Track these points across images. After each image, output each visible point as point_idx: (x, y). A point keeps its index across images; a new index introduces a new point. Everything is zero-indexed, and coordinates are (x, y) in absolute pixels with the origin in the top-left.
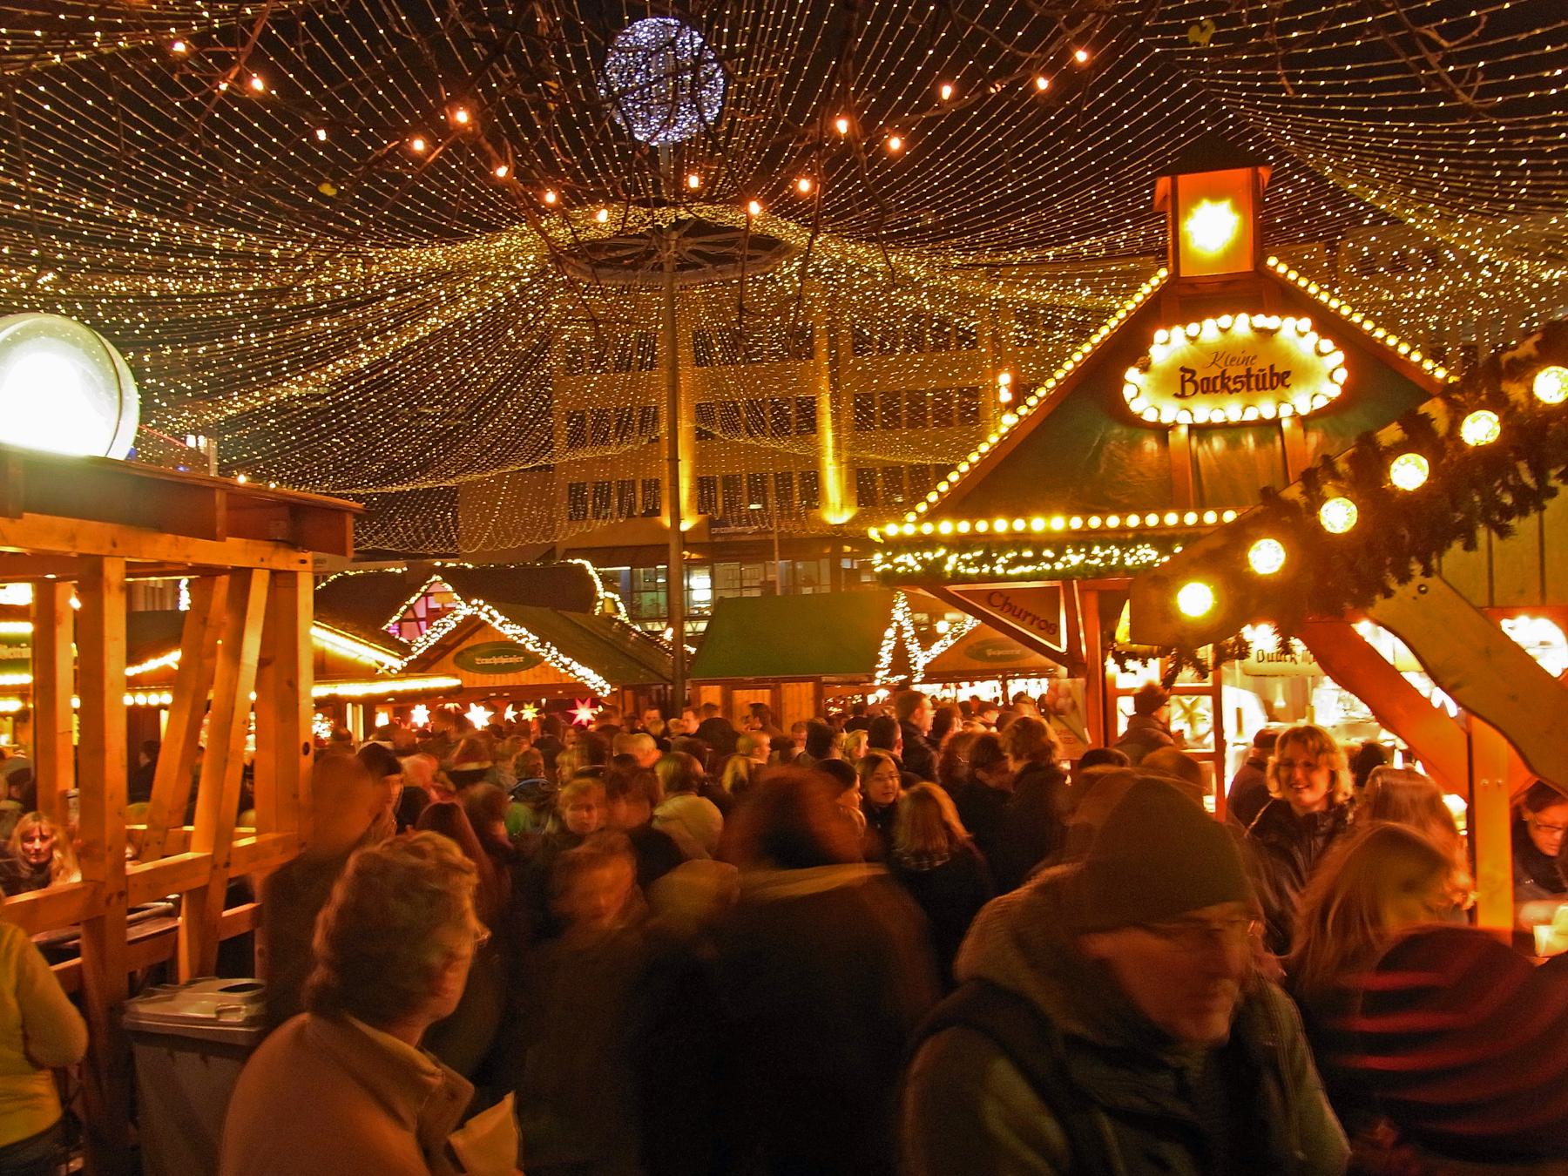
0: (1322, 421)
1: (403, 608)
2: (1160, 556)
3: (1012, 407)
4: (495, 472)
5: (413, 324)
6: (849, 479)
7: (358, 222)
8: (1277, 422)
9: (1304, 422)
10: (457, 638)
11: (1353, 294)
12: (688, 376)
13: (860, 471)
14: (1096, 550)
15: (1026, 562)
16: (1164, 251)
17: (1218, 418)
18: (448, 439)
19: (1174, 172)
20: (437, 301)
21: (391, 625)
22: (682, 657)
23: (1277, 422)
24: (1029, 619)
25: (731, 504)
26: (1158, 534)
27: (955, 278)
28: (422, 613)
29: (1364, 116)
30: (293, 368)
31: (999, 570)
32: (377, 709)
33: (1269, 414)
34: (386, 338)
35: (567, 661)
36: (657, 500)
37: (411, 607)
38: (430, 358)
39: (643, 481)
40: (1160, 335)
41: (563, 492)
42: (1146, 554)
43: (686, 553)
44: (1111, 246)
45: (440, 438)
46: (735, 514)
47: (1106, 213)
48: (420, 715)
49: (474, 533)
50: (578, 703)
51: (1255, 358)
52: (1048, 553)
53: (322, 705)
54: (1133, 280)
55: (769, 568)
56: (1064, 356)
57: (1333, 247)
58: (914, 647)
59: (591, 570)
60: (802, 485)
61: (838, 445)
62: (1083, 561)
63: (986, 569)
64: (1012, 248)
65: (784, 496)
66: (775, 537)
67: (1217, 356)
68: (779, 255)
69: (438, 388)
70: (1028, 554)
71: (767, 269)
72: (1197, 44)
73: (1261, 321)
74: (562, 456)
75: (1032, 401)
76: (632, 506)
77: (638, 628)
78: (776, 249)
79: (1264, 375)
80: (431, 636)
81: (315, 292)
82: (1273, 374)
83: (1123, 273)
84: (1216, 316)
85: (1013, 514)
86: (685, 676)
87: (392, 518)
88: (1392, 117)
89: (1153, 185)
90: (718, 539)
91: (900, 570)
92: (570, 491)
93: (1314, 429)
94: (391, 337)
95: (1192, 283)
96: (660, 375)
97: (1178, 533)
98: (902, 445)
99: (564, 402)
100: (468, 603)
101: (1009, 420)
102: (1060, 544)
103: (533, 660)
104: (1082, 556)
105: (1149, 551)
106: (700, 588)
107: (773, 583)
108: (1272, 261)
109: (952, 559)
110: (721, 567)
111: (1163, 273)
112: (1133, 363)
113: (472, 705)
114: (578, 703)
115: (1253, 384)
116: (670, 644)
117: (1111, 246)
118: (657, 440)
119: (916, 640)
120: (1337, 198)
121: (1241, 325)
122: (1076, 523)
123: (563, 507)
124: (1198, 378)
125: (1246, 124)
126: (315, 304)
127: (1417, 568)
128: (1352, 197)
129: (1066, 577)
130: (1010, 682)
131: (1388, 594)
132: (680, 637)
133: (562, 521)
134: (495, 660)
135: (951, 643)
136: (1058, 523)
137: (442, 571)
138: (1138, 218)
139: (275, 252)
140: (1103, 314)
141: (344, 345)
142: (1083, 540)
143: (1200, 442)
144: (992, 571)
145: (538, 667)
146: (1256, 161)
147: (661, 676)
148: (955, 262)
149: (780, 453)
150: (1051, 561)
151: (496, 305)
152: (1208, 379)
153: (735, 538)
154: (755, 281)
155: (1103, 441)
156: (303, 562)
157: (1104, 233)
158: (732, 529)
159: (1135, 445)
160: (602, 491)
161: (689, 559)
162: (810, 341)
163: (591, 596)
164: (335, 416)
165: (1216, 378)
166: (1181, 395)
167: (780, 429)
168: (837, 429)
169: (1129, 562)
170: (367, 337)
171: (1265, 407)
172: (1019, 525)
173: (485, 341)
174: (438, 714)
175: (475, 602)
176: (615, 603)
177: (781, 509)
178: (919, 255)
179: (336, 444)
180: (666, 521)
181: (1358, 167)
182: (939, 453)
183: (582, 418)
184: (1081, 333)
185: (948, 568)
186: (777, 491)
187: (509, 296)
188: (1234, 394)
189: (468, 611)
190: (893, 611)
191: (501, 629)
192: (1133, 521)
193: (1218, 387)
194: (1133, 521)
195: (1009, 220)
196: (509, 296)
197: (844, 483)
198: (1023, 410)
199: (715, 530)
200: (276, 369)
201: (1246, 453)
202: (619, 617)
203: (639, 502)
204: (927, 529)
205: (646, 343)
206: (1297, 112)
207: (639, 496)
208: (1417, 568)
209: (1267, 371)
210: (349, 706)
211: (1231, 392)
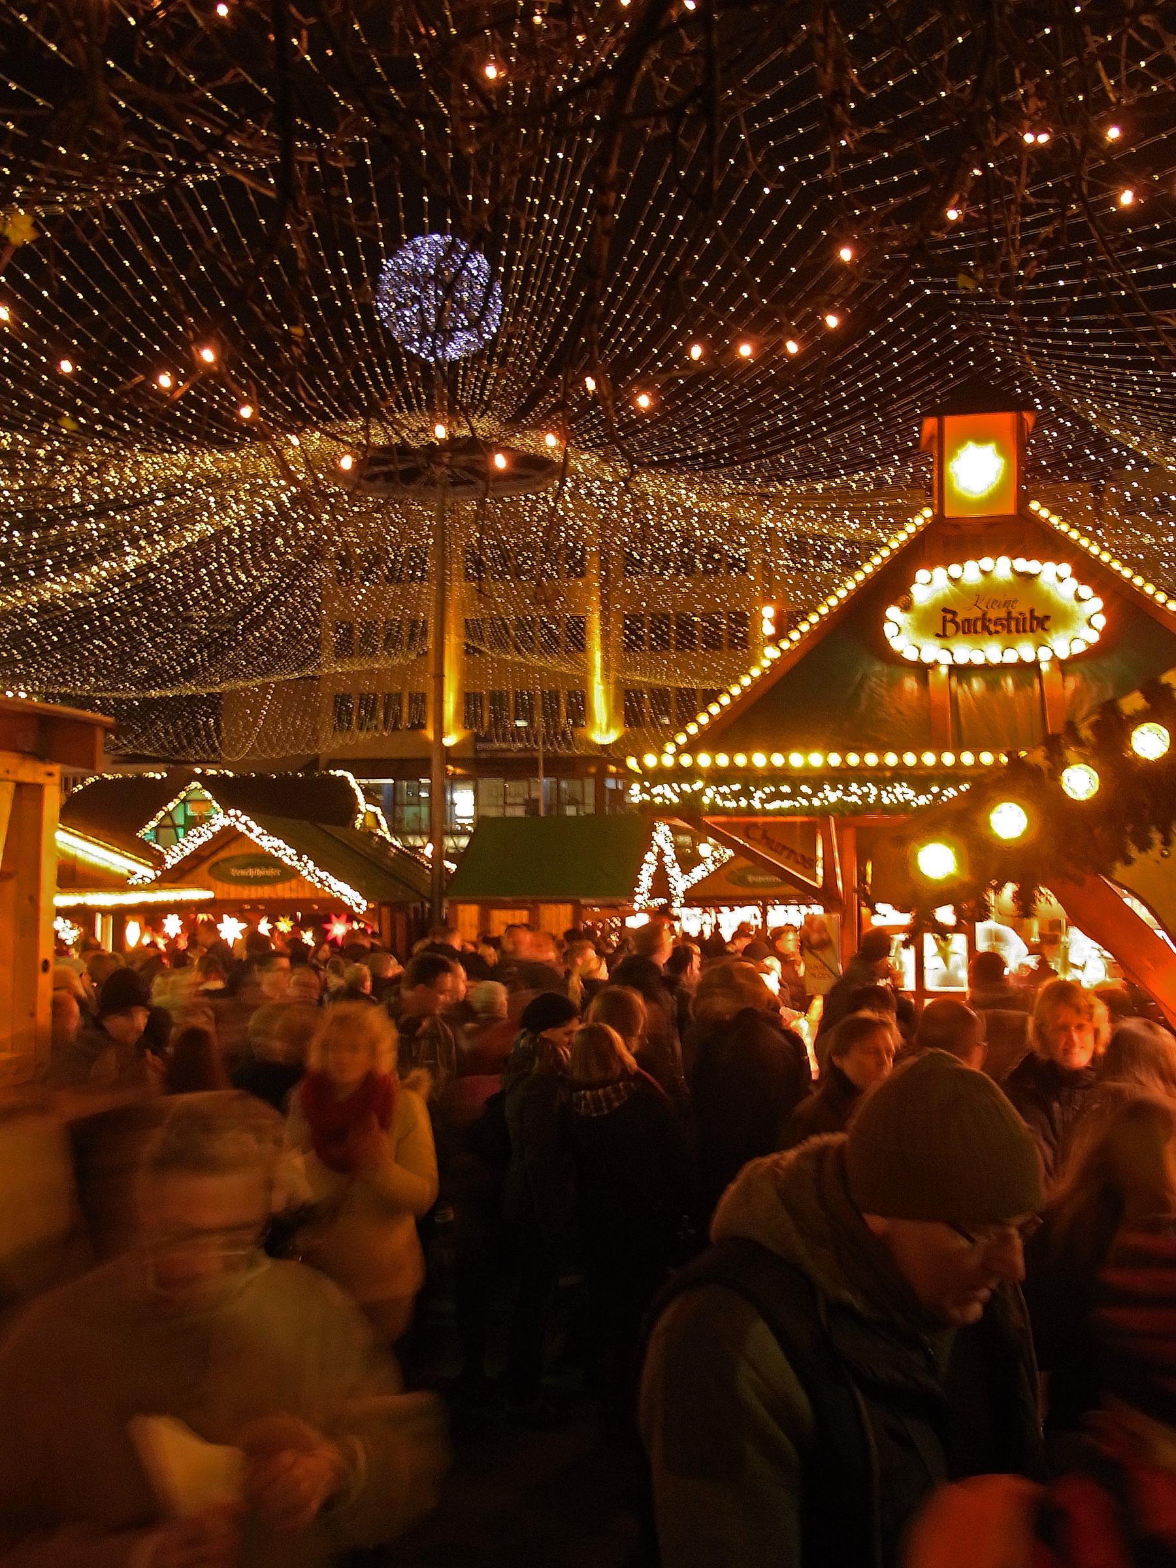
0: (1080, 666)
1: (161, 814)
3: (774, 640)
4: (259, 681)
5: (183, 528)
6: (616, 700)
7: (126, 426)
8: (1036, 664)
9: (1063, 666)
10: (214, 848)
11: (1117, 536)
12: (458, 590)
13: (627, 692)
14: (854, 787)
16: (930, 488)
17: (978, 659)
18: (214, 647)
19: (939, 412)
20: (206, 506)
21: (146, 832)
22: (441, 877)
23: (1036, 664)
25: (497, 721)
26: (915, 773)
27: (725, 505)
28: (180, 820)
29: (1125, 365)
30: (57, 569)
31: (757, 804)
32: (128, 918)
33: (1029, 657)
34: (153, 543)
35: (323, 875)
36: (422, 714)
37: (169, 814)
38: (198, 564)
39: (410, 695)
40: (922, 575)
41: (328, 703)
42: (903, 792)
43: (450, 768)
45: (204, 644)
46: (500, 732)
47: (875, 449)
48: (173, 925)
49: (238, 740)
50: (334, 918)
51: (1016, 601)
52: (805, 789)
53: (65, 913)
54: (901, 515)
55: (533, 786)
56: (829, 588)
57: (1096, 490)
58: (675, 872)
59: (353, 782)
60: (570, 703)
61: (606, 666)
62: (840, 799)
63: (743, 803)
64: (782, 479)
65: (552, 715)
66: (540, 756)
67: (978, 596)
69: (204, 594)
70: (786, 789)
71: (538, 488)
72: (965, 289)
73: (1021, 565)
74: (332, 667)
75: (795, 635)
76: (398, 719)
77: (398, 844)
78: (549, 470)
79: (1024, 619)
80: (190, 844)
81: (81, 493)
82: (1033, 617)
83: (891, 508)
84: (978, 558)
85: (770, 750)
86: (443, 894)
87: (153, 723)
88: (1154, 366)
89: (919, 425)
90: (483, 755)
91: (658, 800)
92: (336, 701)
93: (1073, 674)
94: (158, 542)
95: (956, 523)
96: (428, 589)
97: (935, 772)
98: (669, 669)
99: (331, 611)
100: (226, 813)
101: (772, 653)
102: (817, 780)
103: (290, 874)
104: (839, 793)
105: (906, 790)
106: (464, 803)
107: (537, 801)
109: (710, 792)
110: (484, 783)
111: (928, 513)
112: (894, 602)
113: (225, 917)
114: (334, 918)
115: (1013, 627)
116: (429, 861)
117: (879, 482)
118: (425, 653)
119: (676, 865)
120: (1100, 444)
121: (1002, 568)
122: (835, 759)
123: (328, 719)
125: (1014, 367)
126: (81, 506)
127: (1156, 837)
128: (1115, 442)
129: (825, 812)
130: (769, 908)
131: (1128, 861)
132: (440, 854)
133: (326, 733)
134: (251, 872)
135: (712, 868)
136: (816, 759)
137: (202, 778)
138: (906, 454)
139: (41, 452)
140: (876, 545)
141: (111, 547)
142: (841, 777)
143: (960, 682)
144: (749, 804)
145: (294, 882)
146: (1021, 405)
147: (418, 892)
148: (726, 491)
149: (547, 671)
150: (807, 797)
151: (266, 513)
152: (968, 620)
153: (500, 755)
154: (527, 499)
155: (865, 677)
156: (50, 774)
157: (873, 468)
158: (497, 745)
159: (896, 683)
160: (370, 703)
161: (454, 774)
162: (580, 563)
163: (353, 810)
164: (100, 618)
166: (942, 635)
167: (551, 645)
168: (605, 649)
169: (886, 801)
170: (134, 542)
171: (1025, 651)
172: (778, 760)
173: (252, 550)
174: (189, 926)
175: (232, 812)
176: (375, 815)
177: (547, 727)
178: (690, 482)
179: (98, 647)
180: (430, 734)
181: (1121, 415)
182: (707, 677)
183: (350, 630)
184: (850, 565)
185: (706, 800)
186: (544, 708)
187: (279, 505)
189: (226, 822)
190: (654, 834)
191: (257, 841)
192: (891, 759)
193: (979, 628)
194: (891, 759)
195: (779, 451)
196: (279, 505)
197: (612, 704)
198: (785, 645)
199: (480, 746)
200: (40, 569)
201: (1006, 696)
202: (380, 833)
203: (405, 715)
204: (686, 760)
205: (416, 558)
206: (1062, 357)
207: (405, 709)
208: (1156, 837)
209: (1028, 615)
210: (99, 917)
211: (990, 633)
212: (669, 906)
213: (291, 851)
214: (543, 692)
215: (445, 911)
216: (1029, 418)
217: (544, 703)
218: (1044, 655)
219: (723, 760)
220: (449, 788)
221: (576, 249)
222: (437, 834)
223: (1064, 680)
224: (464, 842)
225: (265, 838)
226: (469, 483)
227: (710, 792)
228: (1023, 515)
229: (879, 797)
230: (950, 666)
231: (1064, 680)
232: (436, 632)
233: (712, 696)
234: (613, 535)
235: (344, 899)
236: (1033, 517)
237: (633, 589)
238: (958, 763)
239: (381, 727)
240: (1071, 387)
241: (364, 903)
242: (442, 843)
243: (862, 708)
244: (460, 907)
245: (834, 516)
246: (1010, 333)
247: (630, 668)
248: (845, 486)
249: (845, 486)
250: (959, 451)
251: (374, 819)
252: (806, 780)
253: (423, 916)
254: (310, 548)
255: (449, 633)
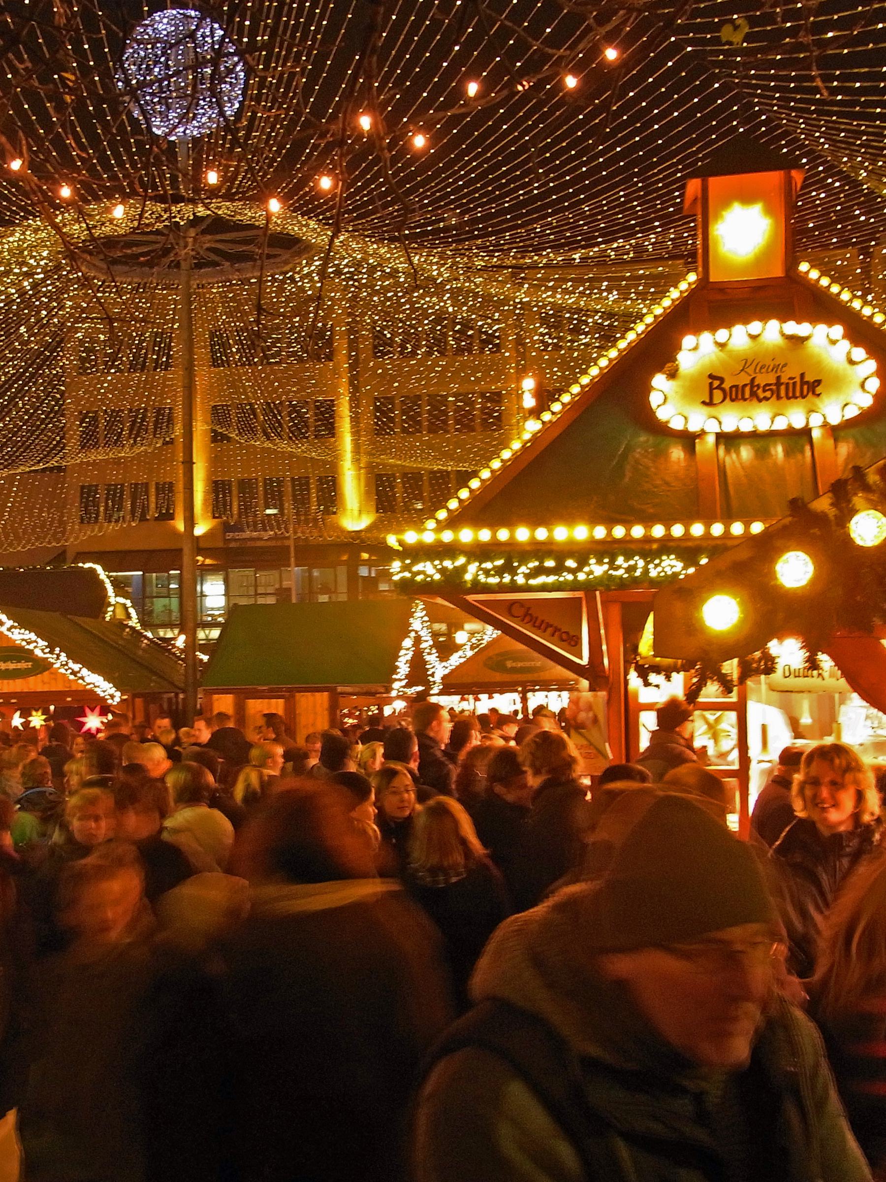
0: (854, 431)
2: (685, 568)
3: (536, 413)
6: (367, 485)
8: (806, 432)
9: (834, 432)
12: (204, 376)
13: (379, 477)
14: (620, 560)
15: (548, 572)
16: (693, 254)
17: (746, 427)
19: (704, 174)
23: (806, 432)
24: (550, 630)
25: (246, 508)
35: (76, 667)
36: (170, 504)
39: (157, 484)
40: (688, 341)
41: (74, 493)
43: (200, 558)
44: (639, 249)
46: (250, 519)
50: (88, 710)
51: (785, 365)
52: (571, 563)
56: (588, 361)
58: (432, 658)
59: (102, 574)
60: (320, 489)
62: (606, 572)
64: (537, 250)
65: (301, 501)
66: (291, 543)
67: (747, 363)
68: (299, 254)
70: (550, 563)
73: (792, 328)
75: (556, 407)
76: (145, 509)
77: (149, 635)
78: (296, 248)
79: (794, 383)
82: (803, 383)
84: (746, 321)
85: (535, 522)
86: (197, 684)
89: (683, 187)
91: (419, 578)
92: (82, 493)
93: (845, 439)
95: (722, 288)
96: (175, 375)
99: (77, 402)
103: (42, 666)
104: (606, 567)
105: (674, 562)
108: (804, 267)
109: (473, 568)
111: (692, 277)
112: (660, 369)
114: (88, 710)
115: (783, 393)
116: (182, 651)
117: (639, 249)
119: (434, 651)
122: (600, 532)
123: (74, 510)
124: (727, 385)
129: (589, 588)
130: (530, 695)
132: (192, 645)
133: (73, 524)
135: (470, 653)
136: (581, 532)
138: (667, 221)
140: (629, 319)
143: (728, 451)
145: (46, 673)
146: (788, 164)
147: (172, 683)
150: (573, 571)
152: (736, 386)
153: (250, 544)
154: (274, 280)
155: (629, 449)
157: (632, 235)
158: (247, 534)
159: (661, 454)
160: (115, 494)
163: (102, 602)
165: (745, 385)
166: (709, 403)
167: (298, 433)
172: (541, 534)
178: (442, 256)
180: (180, 525)
183: (95, 419)
184: (608, 338)
185: (468, 577)
186: (294, 496)
187: (22, 293)
188: (764, 402)
191: (9, 634)
192: (658, 531)
193: (747, 395)
195: (536, 220)
196: (22, 293)
199: (230, 535)
201: (775, 464)
202: (130, 623)
203: (153, 506)
204: (447, 536)
205: (162, 343)
207: (153, 499)
209: (798, 380)
211: (760, 400)
212: (425, 694)
213: (42, 643)
214: (293, 479)
215: (199, 701)
216: (798, 176)
217: (294, 490)
218: (816, 421)
219: (485, 535)
220: (199, 579)
221: (322, 17)
222: (191, 625)
223: (836, 447)
224: (215, 633)
225: (16, 631)
226: (216, 264)
227: (473, 568)
228: (792, 278)
229: (646, 571)
230: (717, 434)
231: (836, 447)
232: (184, 415)
233: (463, 479)
234: (363, 314)
235: (97, 690)
236: (802, 281)
237: (385, 370)
238: (727, 534)
239: (128, 517)
240: (839, 145)
241: (118, 694)
242: (194, 634)
243: (627, 480)
244: (216, 696)
245: (591, 288)
246: (776, 89)
247: (384, 451)
248: (603, 253)
249: (603, 253)
250: (724, 213)
251: (124, 612)
252: (571, 554)
253: (177, 708)
254: (54, 335)
255: (196, 421)
